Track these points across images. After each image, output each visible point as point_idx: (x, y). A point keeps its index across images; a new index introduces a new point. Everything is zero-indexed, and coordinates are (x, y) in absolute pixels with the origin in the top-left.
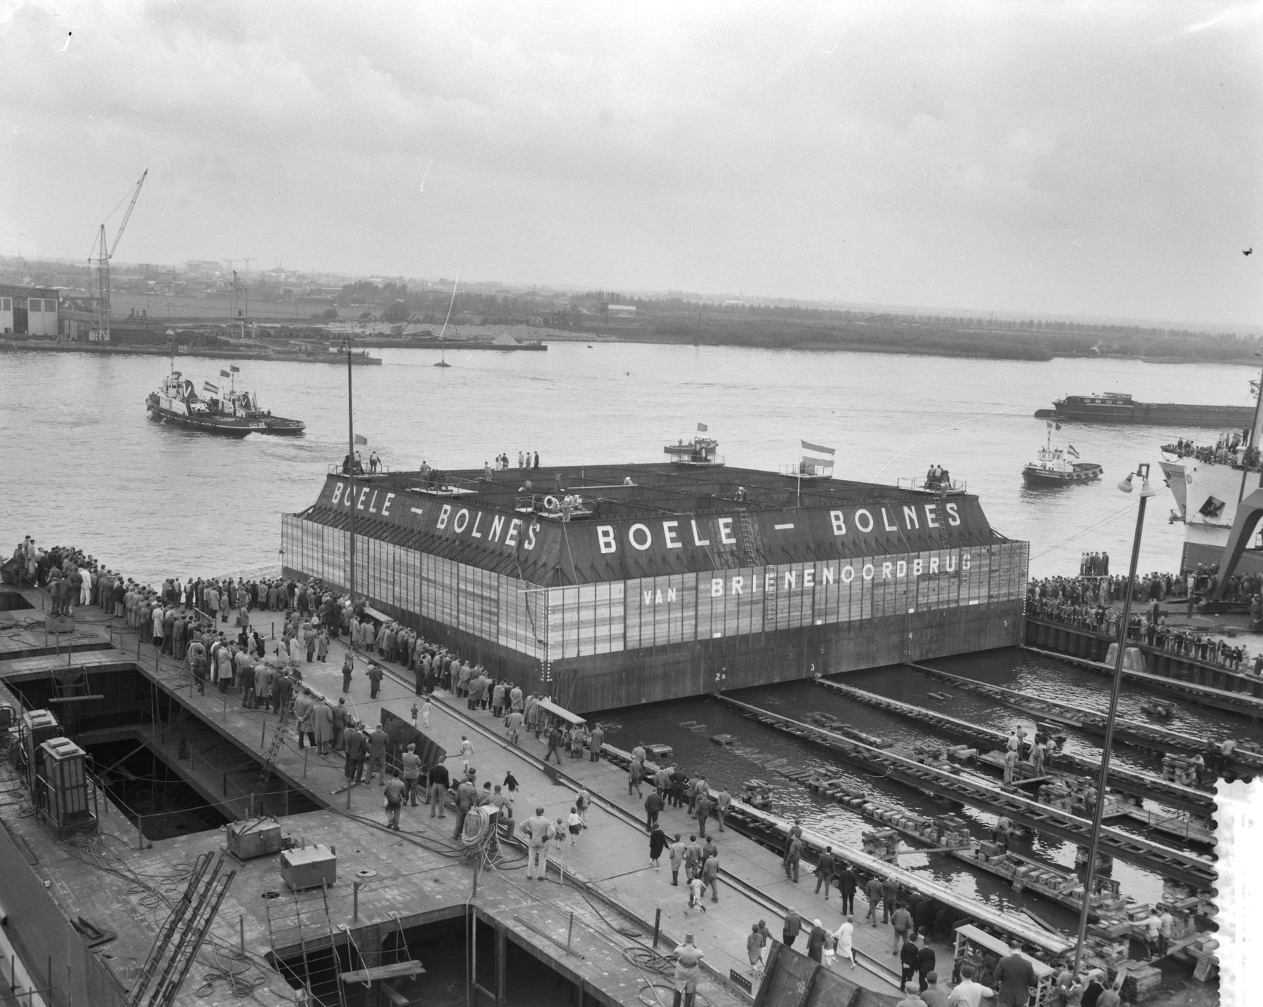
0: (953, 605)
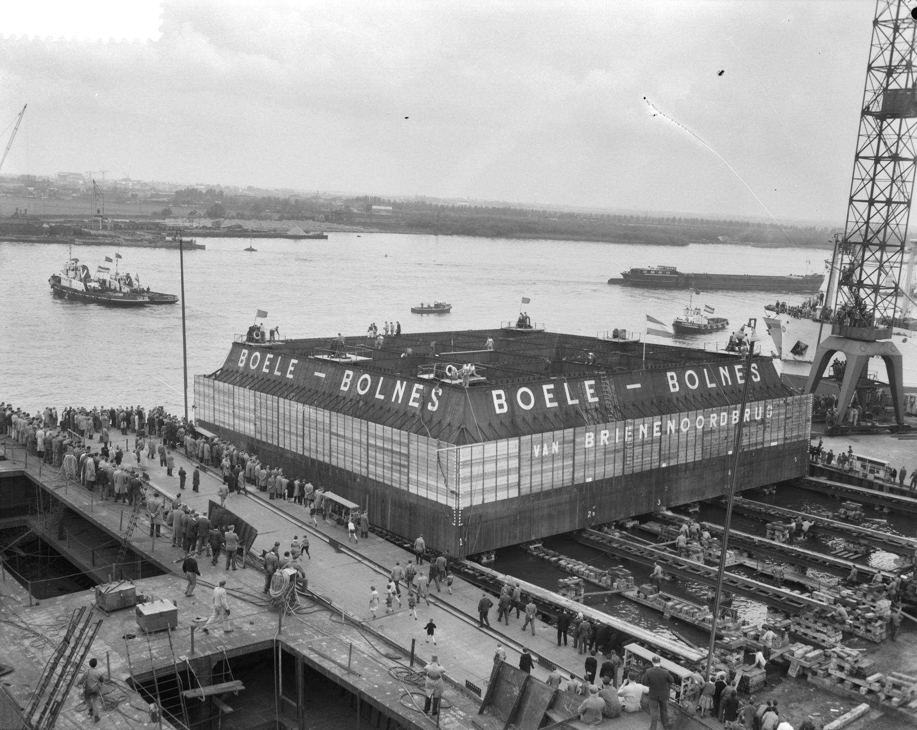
0: (759, 447)
